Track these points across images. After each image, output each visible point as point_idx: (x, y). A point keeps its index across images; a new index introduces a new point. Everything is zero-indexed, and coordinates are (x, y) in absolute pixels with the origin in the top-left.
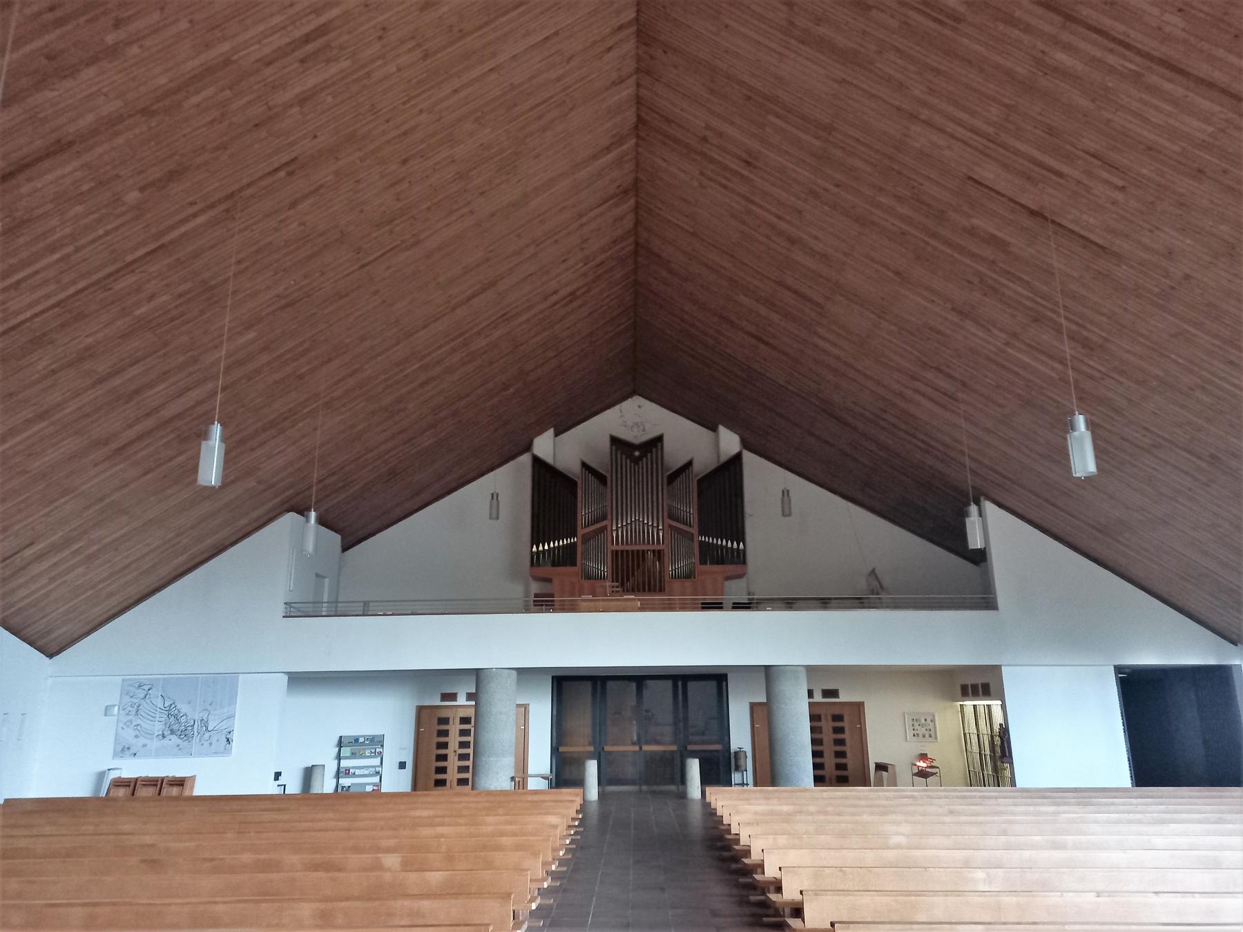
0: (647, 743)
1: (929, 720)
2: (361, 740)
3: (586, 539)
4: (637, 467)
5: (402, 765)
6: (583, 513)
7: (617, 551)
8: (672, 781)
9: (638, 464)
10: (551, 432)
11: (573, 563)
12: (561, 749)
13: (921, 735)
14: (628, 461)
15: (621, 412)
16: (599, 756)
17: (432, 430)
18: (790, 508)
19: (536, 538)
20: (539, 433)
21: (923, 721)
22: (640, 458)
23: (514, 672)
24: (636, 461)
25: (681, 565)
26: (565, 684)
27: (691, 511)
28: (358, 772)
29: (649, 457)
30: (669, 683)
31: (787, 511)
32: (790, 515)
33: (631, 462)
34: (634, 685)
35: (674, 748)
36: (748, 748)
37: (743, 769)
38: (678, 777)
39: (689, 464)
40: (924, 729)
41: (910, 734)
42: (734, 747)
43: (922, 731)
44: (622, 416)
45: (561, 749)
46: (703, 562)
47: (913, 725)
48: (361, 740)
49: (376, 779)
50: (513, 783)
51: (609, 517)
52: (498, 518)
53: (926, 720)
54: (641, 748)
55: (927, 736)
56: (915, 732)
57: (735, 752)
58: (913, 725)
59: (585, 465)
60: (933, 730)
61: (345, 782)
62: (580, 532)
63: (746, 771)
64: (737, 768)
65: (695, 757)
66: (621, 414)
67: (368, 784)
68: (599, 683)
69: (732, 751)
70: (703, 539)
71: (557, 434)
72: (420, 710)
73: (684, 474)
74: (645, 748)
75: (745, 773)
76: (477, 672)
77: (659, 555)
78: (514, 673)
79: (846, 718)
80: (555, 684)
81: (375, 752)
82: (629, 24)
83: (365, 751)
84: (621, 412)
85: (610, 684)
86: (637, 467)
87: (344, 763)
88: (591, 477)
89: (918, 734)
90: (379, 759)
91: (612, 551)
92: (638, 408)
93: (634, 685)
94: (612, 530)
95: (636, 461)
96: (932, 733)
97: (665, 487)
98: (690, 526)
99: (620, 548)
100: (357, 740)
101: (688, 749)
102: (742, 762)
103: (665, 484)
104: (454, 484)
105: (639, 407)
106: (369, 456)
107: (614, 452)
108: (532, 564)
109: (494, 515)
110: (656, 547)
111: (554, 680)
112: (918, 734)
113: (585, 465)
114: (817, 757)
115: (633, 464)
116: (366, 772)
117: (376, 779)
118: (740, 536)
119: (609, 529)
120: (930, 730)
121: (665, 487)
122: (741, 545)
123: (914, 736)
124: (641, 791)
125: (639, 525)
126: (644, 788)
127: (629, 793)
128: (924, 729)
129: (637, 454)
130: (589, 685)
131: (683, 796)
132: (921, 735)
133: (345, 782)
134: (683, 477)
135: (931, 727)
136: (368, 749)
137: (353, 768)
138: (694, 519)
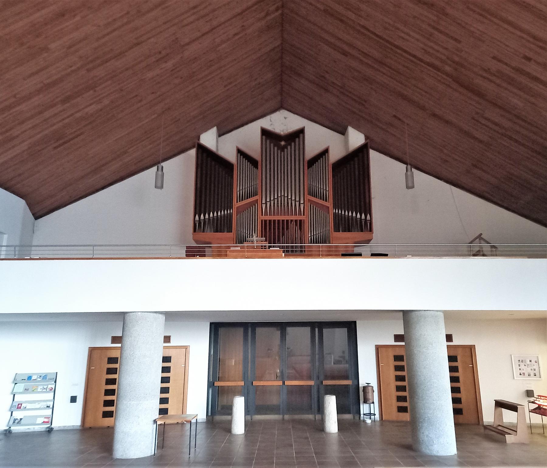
0: (290, 378)
1: (533, 362)
2: (34, 377)
3: (240, 210)
4: (283, 153)
5: (73, 399)
6: (237, 190)
7: (266, 221)
8: (309, 410)
9: (284, 151)
10: (214, 130)
11: (230, 230)
12: (217, 384)
13: (526, 374)
14: (276, 148)
15: (271, 121)
16: (245, 392)
17: (91, 92)
18: (413, 183)
19: (199, 208)
20: (206, 130)
21: (528, 362)
22: (285, 147)
23: (160, 316)
24: (282, 149)
25: (318, 232)
26: (222, 331)
27: (328, 189)
28: (29, 406)
29: (293, 147)
30: (308, 330)
31: (410, 185)
32: (413, 187)
33: (278, 150)
34: (345, 330)
35: (312, 383)
36: (374, 384)
37: (371, 401)
38: (315, 406)
39: (326, 152)
40: (529, 369)
41: (516, 372)
42: (362, 382)
43: (527, 370)
44: (271, 124)
45: (217, 384)
46: (337, 229)
47: (519, 365)
48: (34, 377)
49: (49, 412)
50: (155, 425)
51: (260, 193)
52: (162, 187)
53: (530, 361)
54: (284, 383)
55: (532, 375)
56: (522, 372)
57: (364, 387)
58: (519, 365)
59: (240, 152)
60: (537, 369)
61: (18, 415)
62: (236, 204)
63: (373, 403)
64: (365, 402)
65: (331, 393)
66: (271, 123)
67: (41, 416)
68: (250, 329)
69: (360, 386)
70: (337, 211)
71: (220, 134)
72: (92, 350)
73: (321, 159)
74: (288, 383)
75: (372, 405)
76: (122, 316)
77: (300, 224)
78: (162, 318)
79: (459, 358)
80: (213, 330)
81: (46, 389)
82: (278, 46)
83: (38, 387)
84: (271, 121)
85: (259, 330)
86: (283, 153)
87: (18, 398)
88: (246, 163)
89: (524, 374)
90: (50, 396)
91: (262, 221)
92: (284, 119)
93: (278, 333)
94: (262, 203)
95: (282, 149)
96: (537, 372)
97: (306, 171)
98: (326, 201)
99: (268, 218)
100: (30, 378)
101: (243, 382)
102: (370, 396)
103: (306, 167)
104: (133, 168)
105: (285, 118)
106: (23, 107)
107: (264, 142)
108: (195, 230)
109: (159, 184)
110: (298, 218)
111: (213, 326)
112: (524, 374)
113: (240, 152)
114: (456, 403)
115: (279, 151)
116: (37, 406)
117: (49, 412)
118: (367, 209)
119: (259, 203)
120: (535, 370)
121: (306, 171)
122: (368, 216)
123: (520, 374)
124: (283, 419)
125: (284, 199)
126: (287, 417)
127: (275, 421)
128: (529, 369)
129: (283, 143)
130: (241, 330)
131: (320, 427)
132: (526, 374)
133: (18, 415)
134: (320, 161)
135: (536, 367)
136: (41, 385)
137: (26, 402)
138: (330, 194)
